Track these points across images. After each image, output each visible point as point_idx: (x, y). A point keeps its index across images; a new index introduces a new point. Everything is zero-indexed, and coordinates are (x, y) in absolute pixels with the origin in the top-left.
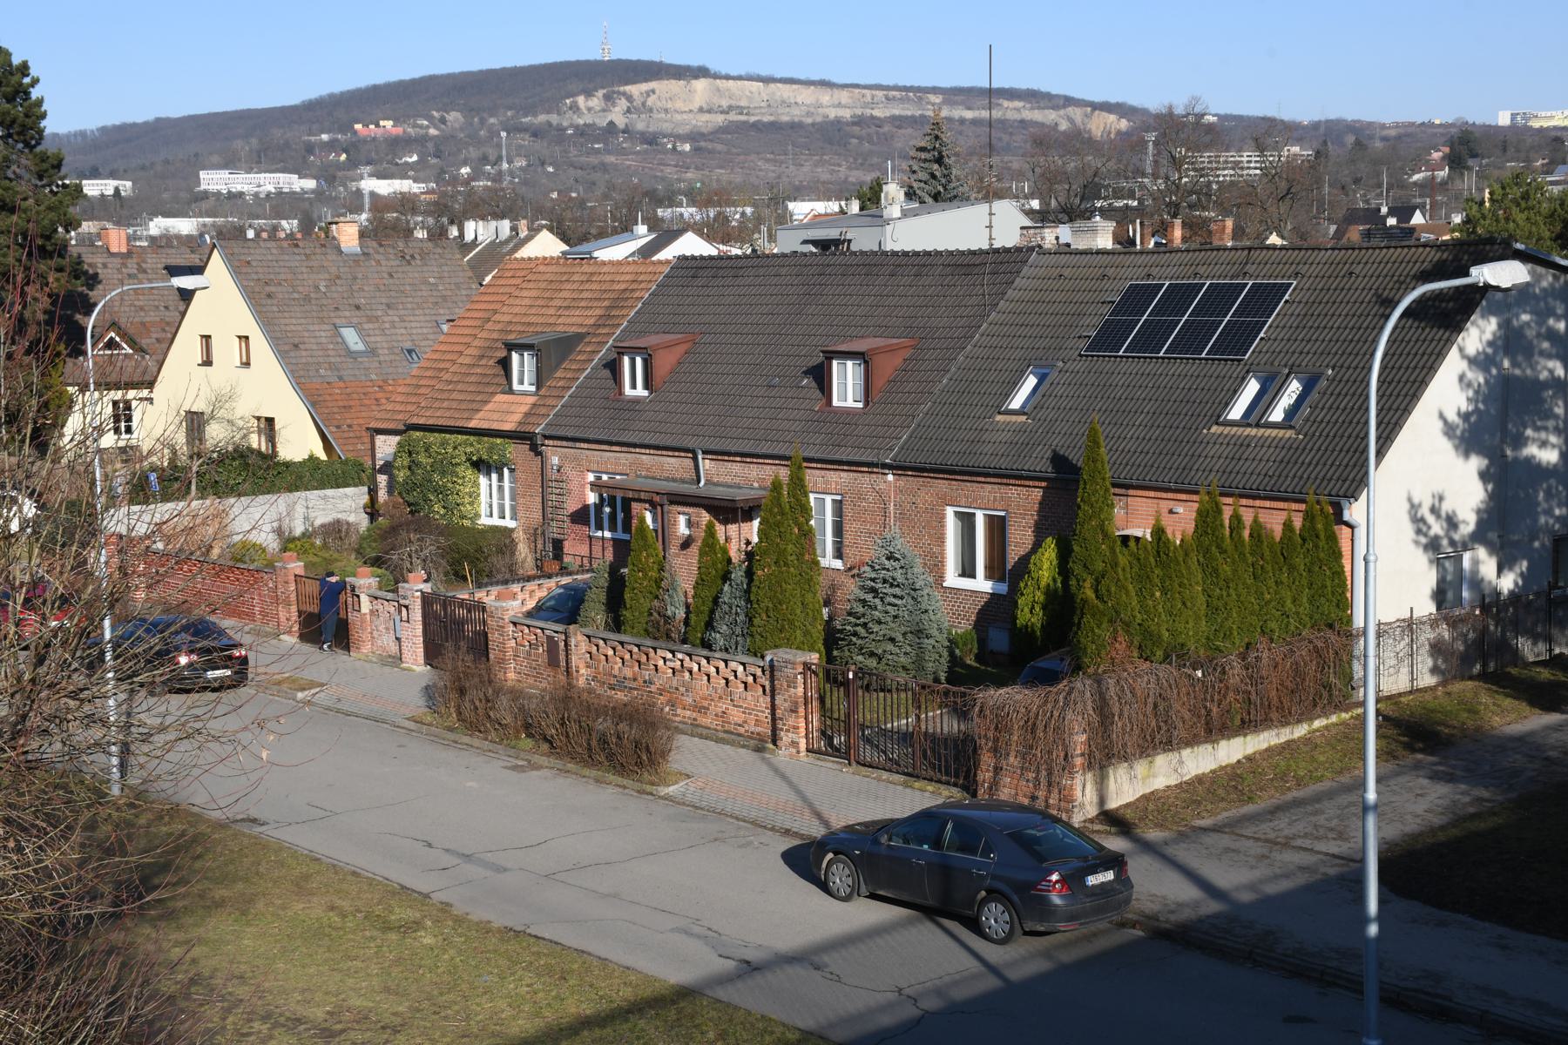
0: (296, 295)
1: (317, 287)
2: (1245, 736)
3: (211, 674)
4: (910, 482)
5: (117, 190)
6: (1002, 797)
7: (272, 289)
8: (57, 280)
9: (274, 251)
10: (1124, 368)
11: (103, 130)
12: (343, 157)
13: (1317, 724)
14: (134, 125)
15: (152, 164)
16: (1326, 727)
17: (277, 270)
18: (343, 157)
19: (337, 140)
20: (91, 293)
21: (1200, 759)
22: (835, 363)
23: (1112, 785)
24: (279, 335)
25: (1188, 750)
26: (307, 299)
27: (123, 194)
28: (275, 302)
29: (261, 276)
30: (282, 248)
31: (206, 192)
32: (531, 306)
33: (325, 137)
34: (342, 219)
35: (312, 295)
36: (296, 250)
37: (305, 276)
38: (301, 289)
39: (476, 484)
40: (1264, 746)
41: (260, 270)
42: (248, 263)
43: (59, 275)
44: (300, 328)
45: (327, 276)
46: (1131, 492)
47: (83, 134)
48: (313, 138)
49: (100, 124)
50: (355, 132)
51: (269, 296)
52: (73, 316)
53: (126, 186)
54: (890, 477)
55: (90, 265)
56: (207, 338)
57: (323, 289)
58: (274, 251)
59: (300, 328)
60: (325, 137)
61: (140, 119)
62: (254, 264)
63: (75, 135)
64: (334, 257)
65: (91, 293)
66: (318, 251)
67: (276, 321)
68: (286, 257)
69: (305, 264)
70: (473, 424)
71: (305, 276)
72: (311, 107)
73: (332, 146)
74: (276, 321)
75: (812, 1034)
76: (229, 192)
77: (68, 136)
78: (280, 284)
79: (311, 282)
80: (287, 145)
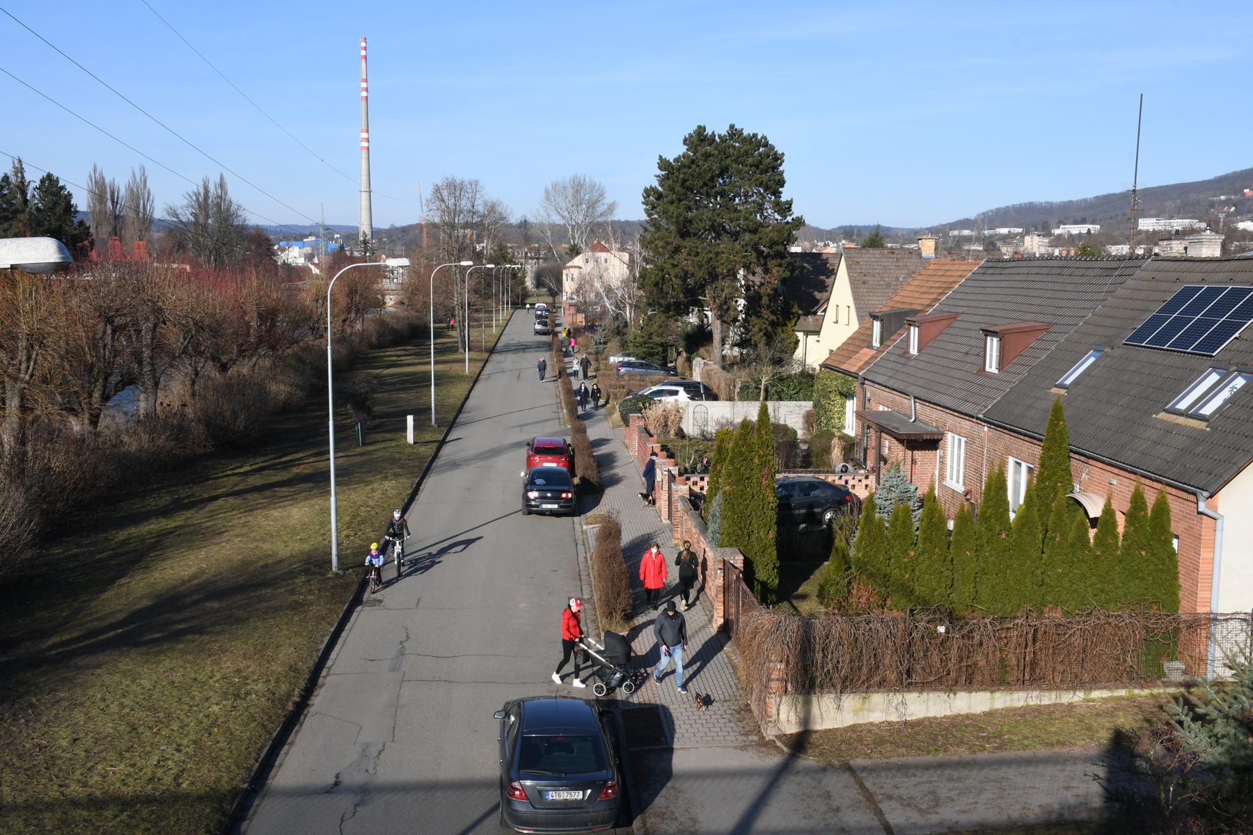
0: (882, 283)
1: (897, 278)
2: (971, 692)
3: (545, 506)
4: (996, 433)
5: (1089, 230)
6: (619, 698)
7: (868, 278)
8: (778, 271)
9: (877, 256)
10: (1144, 355)
11: (1097, 198)
12: (1233, 209)
13: (1096, 694)
14: (1114, 194)
15: (1117, 215)
16: (1105, 700)
17: (875, 267)
18: (1233, 209)
19: (1231, 199)
20: (827, 280)
21: (931, 703)
22: (989, 338)
23: (815, 710)
24: (862, 306)
25: (915, 695)
26: (889, 285)
27: (1092, 232)
28: (866, 286)
29: (863, 271)
30: (883, 254)
31: (1140, 230)
32: (925, 293)
33: (1223, 198)
34: (925, 237)
35: (893, 283)
36: (892, 256)
37: (892, 271)
38: (886, 279)
39: (843, 406)
40: (1021, 704)
41: (864, 267)
42: (858, 262)
43: (779, 268)
44: (877, 302)
45: (907, 272)
46: (1091, 461)
47: (1085, 200)
48: (1215, 199)
49: (1096, 195)
50: (1244, 194)
51: (864, 283)
52: (813, 292)
53: (1095, 228)
54: (986, 429)
55: (831, 264)
56: (837, 306)
57: (901, 279)
58: (877, 256)
59: (877, 302)
60: (1223, 198)
61: (1118, 191)
62: (861, 263)
63: (1081, 201)
64: (916, 260)
65: (827, 280)
66: (906, 256)
67: (863, 298)
68: (884, 260)
69: (896, 264)
70: (844, 367)
71: (892, 271)
72: (1219, 180)
73: (1226, 203)
74: (863, 298)
75: (997, 830)
76: (1154, 230)
77: (1077, 202)
78: (874, 276)
79: (894, 275)
80: (1198, 203)
